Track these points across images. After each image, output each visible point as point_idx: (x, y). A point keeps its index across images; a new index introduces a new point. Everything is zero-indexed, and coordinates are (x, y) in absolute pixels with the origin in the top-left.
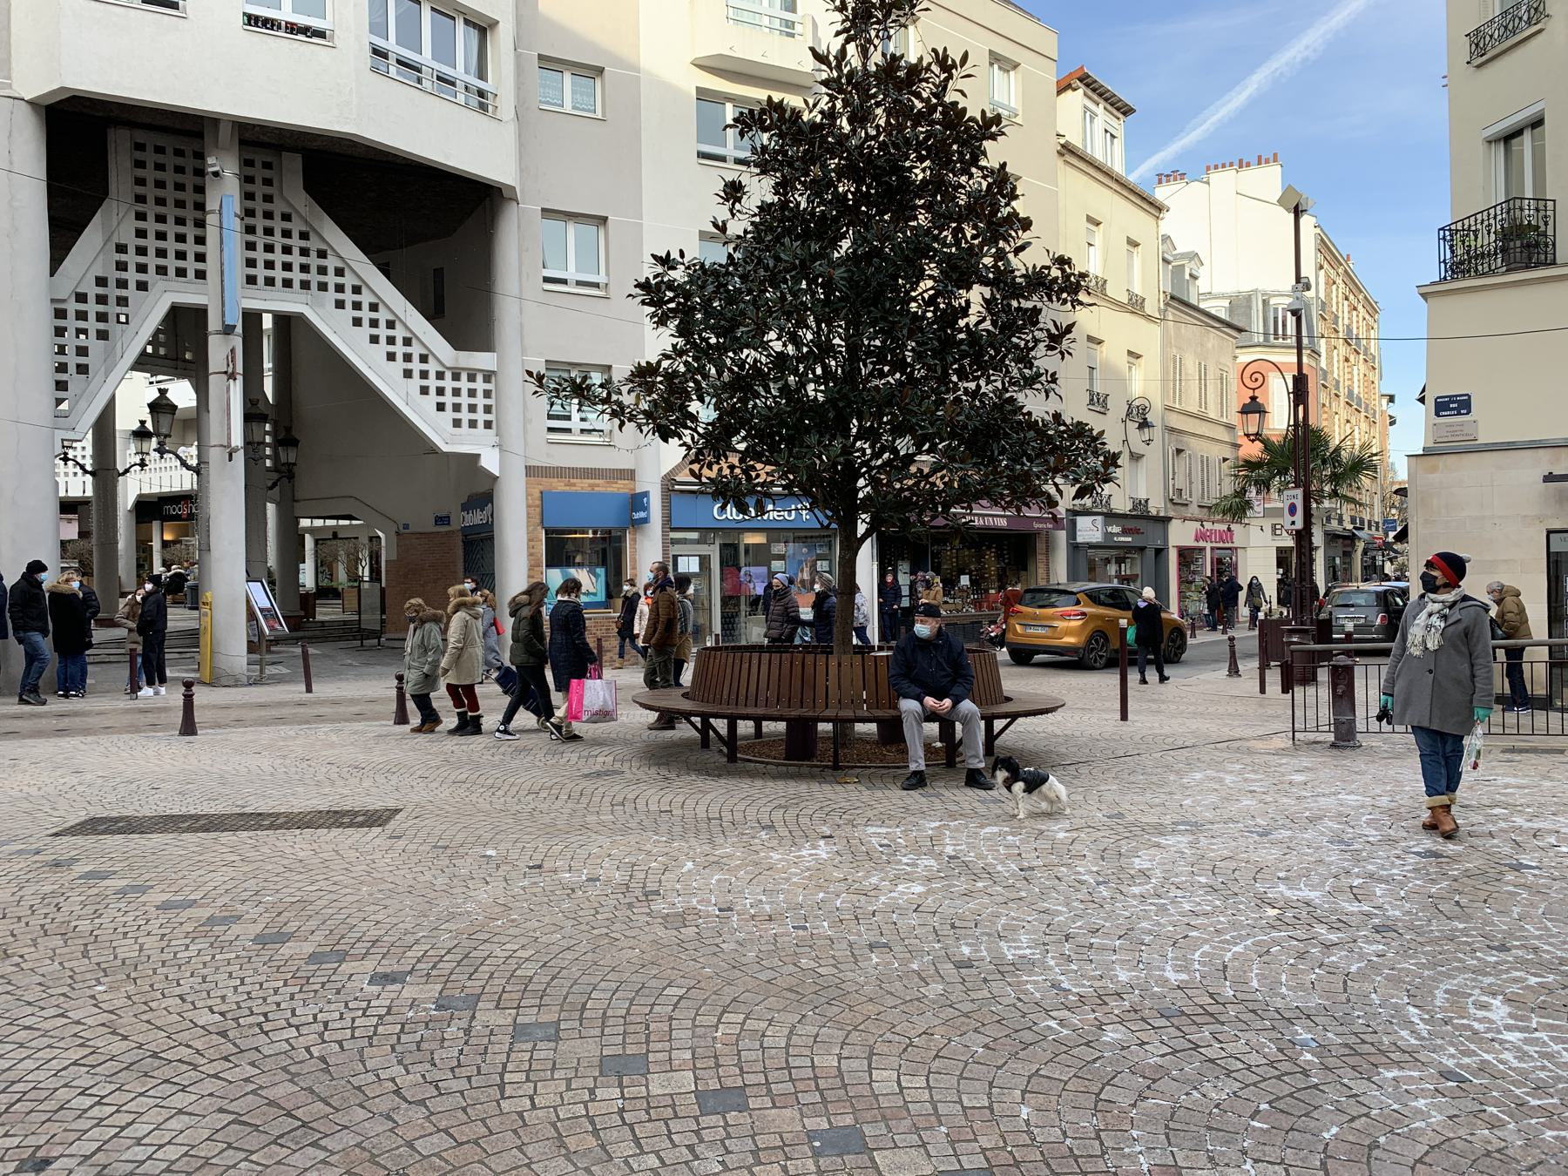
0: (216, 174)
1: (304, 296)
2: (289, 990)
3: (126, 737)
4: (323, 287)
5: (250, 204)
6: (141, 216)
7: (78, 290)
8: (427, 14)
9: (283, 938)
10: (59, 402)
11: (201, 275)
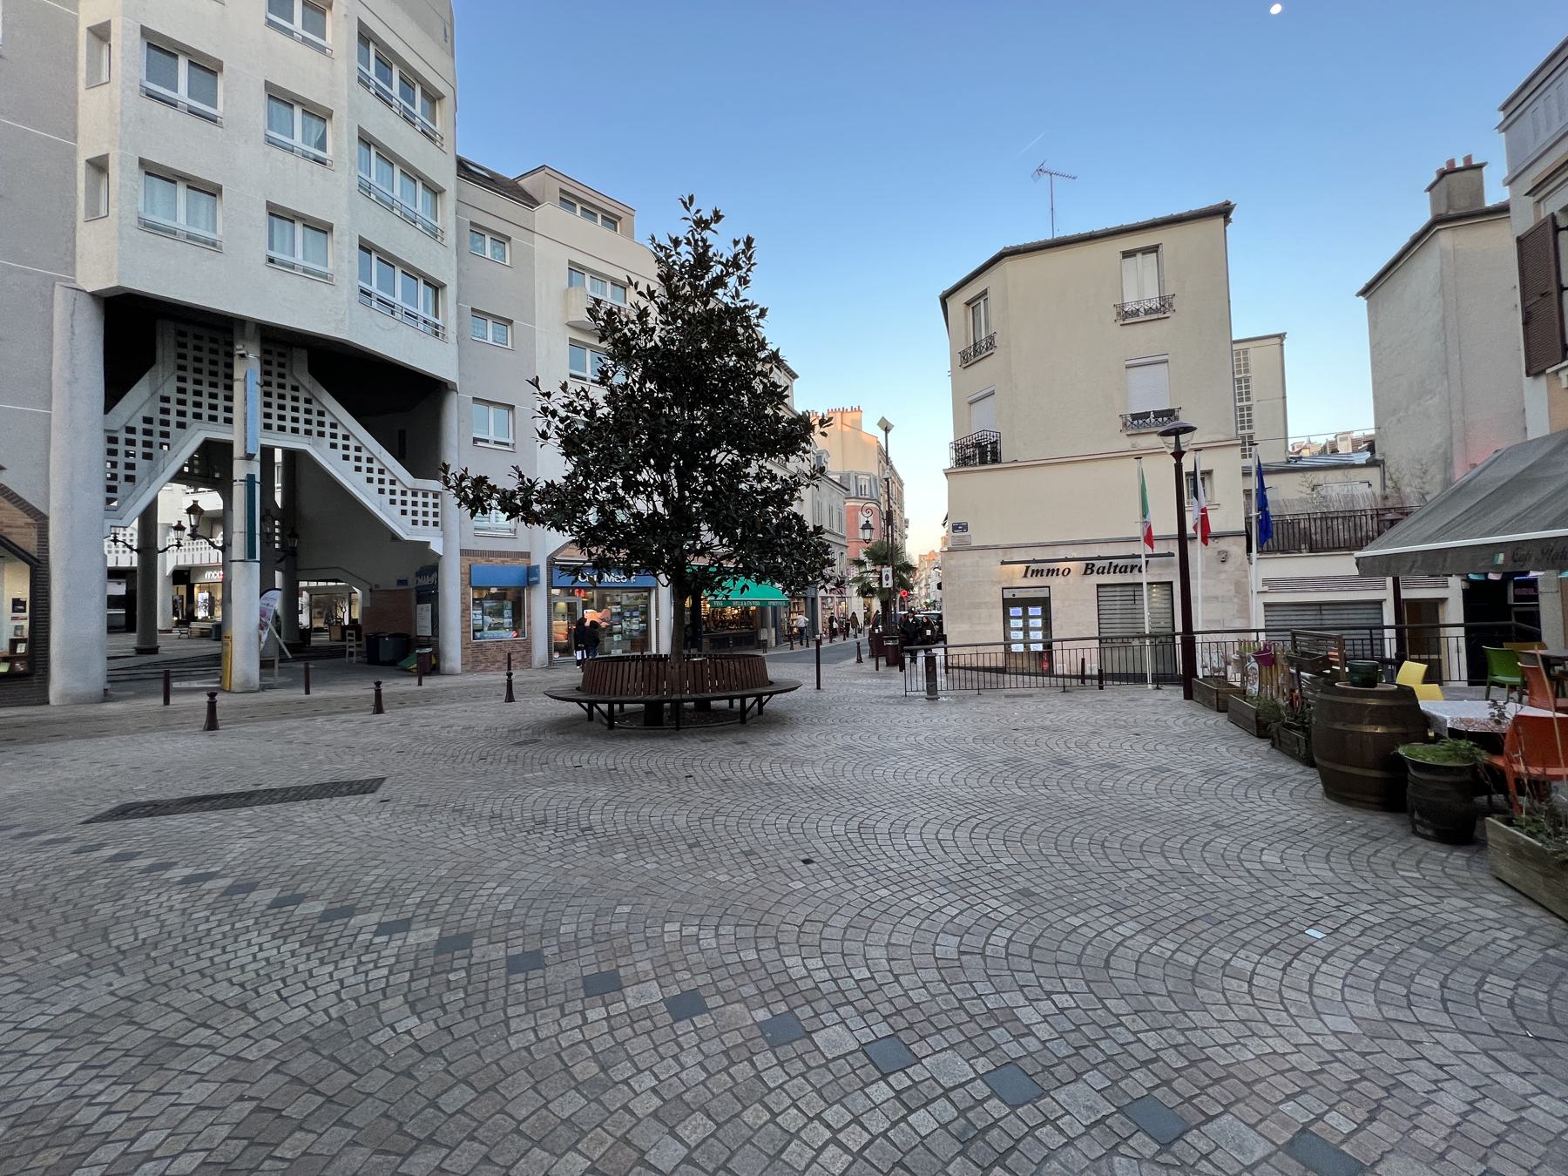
0: (242, 356)
1: (307, 439)
2: (305, 950)
3: (157, 734)
4: (321, 434)
5: (268, 378)
6: (182, 379)
7: (129, 425)
9: (298, 900)
10: (109, 501)
11: (229, 421)
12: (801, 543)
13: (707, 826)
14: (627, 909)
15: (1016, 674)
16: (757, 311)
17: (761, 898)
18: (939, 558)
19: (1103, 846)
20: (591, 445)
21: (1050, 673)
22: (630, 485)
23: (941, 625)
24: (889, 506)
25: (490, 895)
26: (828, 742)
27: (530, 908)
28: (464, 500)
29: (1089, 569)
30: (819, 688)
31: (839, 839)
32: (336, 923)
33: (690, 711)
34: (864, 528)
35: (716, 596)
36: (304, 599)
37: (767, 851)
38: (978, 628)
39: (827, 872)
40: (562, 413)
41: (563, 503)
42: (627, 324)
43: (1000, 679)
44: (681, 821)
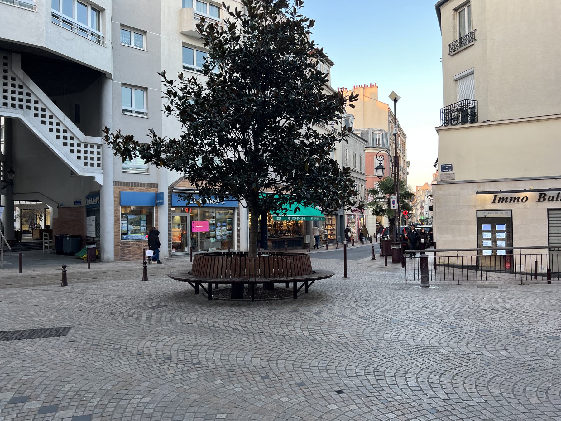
1: (20, 111)
4: (29, 108)
8: (76, 4)
9: (25, 399)
12: (335, 179)
13: (274, 365)
14: (224, 416)
15: (486, 271)
16: (308, 22)
17: (309, 414)
18: (431, 189)
19: (547, 393)
20: (198, 115)
21: (511, 270)
22: (224, 142)
23: (432, 235)
24: (396, 153)
25: (139, 403)
26: (351, 314)
27: (163, 412)
28: (118, 151)
29: (542, 197)
30: (345, 276)
31: (361, 378)
32: (48, 415)
33: (261, 289)
34: (378, 168)
35: (278, 214)
36: (17, 212)
37: (313, 383)
38: (458, 238)
39: (353, 400)
40: (180, 94)
41: (181, 153)
42: (222, 33)
43: (474, 274)
44: (256, 361)
